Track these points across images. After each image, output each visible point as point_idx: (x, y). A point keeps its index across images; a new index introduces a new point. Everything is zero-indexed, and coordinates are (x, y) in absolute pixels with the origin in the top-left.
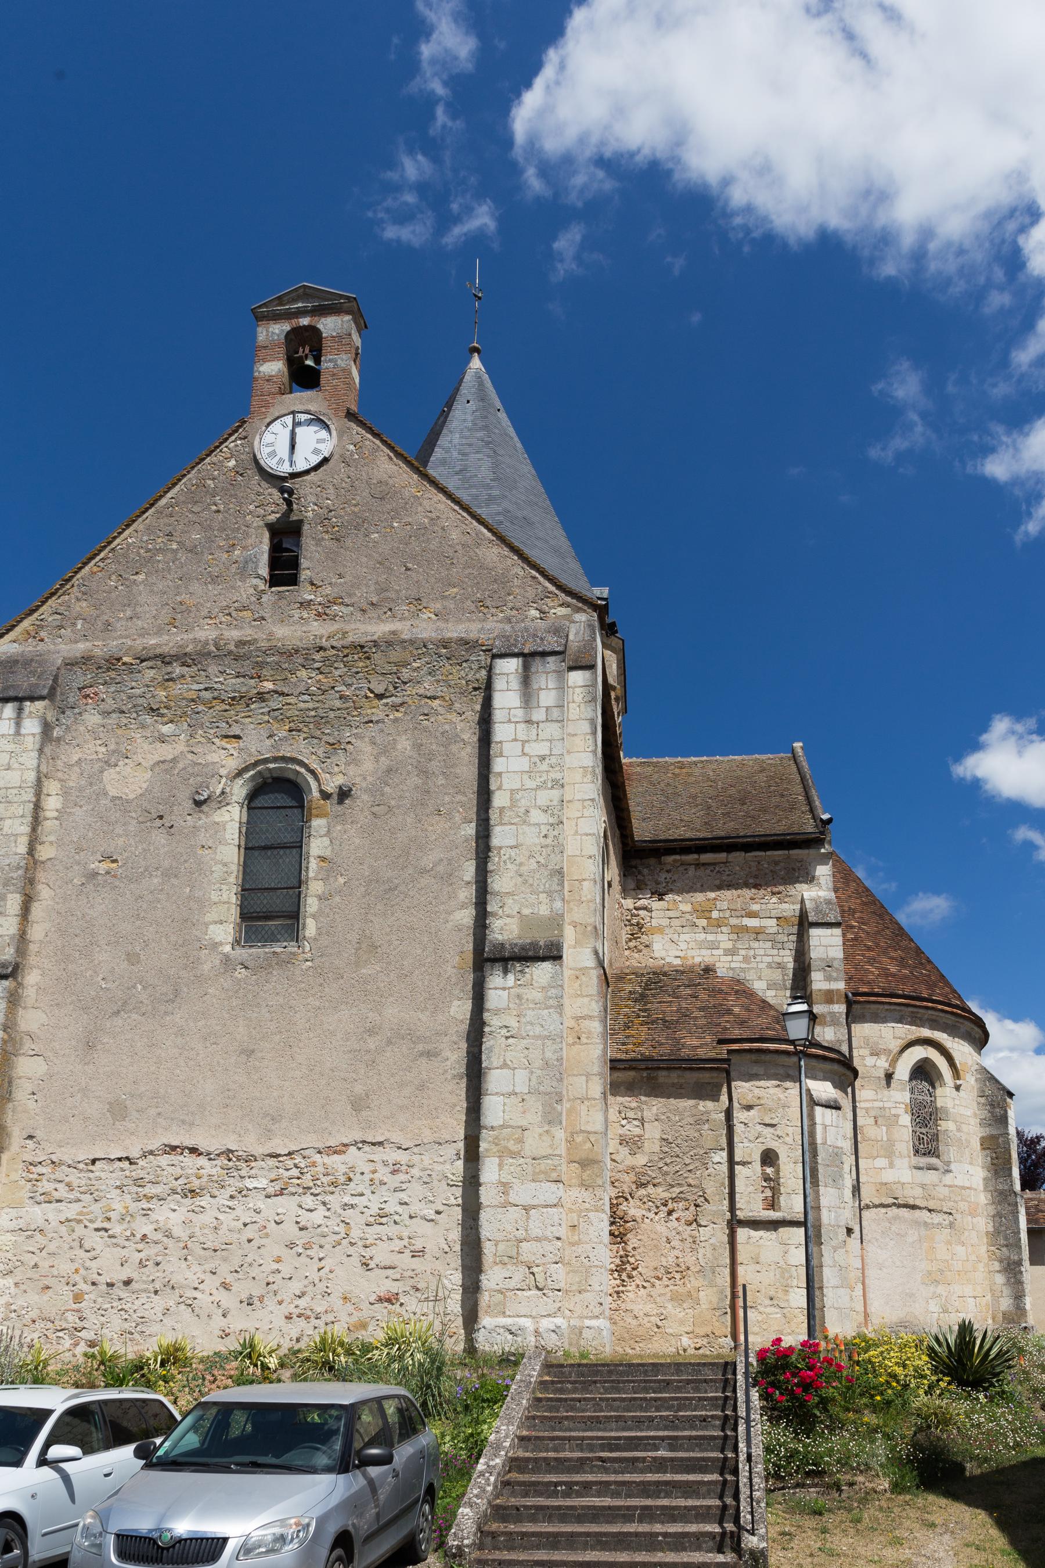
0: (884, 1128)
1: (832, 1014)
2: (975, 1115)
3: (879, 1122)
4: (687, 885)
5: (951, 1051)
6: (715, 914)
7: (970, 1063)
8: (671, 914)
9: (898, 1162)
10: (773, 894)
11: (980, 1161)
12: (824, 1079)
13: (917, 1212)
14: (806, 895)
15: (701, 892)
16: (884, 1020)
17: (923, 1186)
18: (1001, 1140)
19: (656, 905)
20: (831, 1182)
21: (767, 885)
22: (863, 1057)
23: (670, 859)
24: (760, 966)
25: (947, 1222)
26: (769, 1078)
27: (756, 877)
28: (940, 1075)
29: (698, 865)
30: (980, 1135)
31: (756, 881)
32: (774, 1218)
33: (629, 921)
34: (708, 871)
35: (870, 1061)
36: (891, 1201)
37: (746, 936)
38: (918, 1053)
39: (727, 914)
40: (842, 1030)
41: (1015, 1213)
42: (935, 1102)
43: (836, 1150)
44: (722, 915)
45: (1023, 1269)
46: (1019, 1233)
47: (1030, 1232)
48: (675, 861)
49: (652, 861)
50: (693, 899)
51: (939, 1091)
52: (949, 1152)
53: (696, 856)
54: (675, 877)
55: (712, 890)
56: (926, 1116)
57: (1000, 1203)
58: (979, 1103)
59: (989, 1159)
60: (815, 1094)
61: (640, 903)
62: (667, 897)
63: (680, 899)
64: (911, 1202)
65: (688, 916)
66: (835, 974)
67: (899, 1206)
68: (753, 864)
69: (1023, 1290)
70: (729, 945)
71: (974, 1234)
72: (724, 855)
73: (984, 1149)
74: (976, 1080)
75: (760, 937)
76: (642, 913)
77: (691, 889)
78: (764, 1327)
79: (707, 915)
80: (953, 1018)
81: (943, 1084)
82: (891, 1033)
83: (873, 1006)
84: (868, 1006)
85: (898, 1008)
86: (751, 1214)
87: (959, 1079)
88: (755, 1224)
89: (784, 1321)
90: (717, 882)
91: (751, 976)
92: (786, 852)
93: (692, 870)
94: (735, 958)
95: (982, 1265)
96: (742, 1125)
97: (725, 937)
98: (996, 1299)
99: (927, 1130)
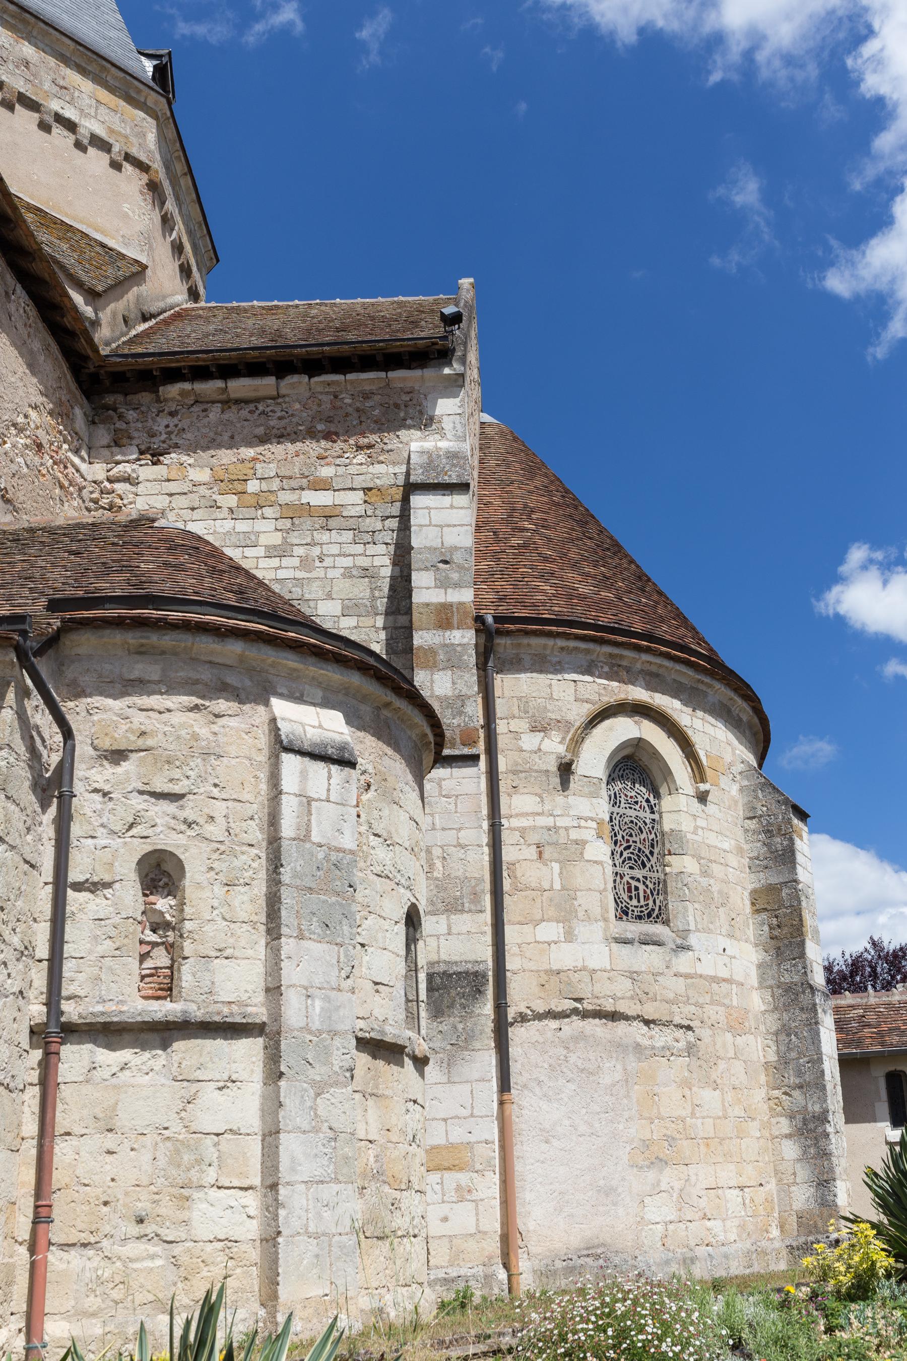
0: (556, 866)
1: (449, 647)
2: (740, 851)
3: (546, 855)
4: (204, 436)
5: (690, 732)
6: (253, 486)
7: (728, 758)
8: (172, 487)
9: (582, 930)
10: (359, 448)
11: (751, 933)
12: (326, 703)
13: (621, 1027)
14: (415, 446)
15: (230, 448)
16: (558, 668)
17: (633, 975)
18: (785, 892)
19: (147, 472)
20: (315, 926)
21: (349, 433)
22: (516, 735)
23: (173, 390)
24: (331, 574)
25: (682, 1044)
26: (172, 689)
27: (329, 420)
28: (667, 773)
29: (227, 403)
30: (750, 887)
31: (329, 427)
32: (159, 1016)
33: (95, 501)
34: (244, 413)
35: (530, 741)
36: (569, 1005)
37: (308, 523)
38: (623, 730)
39: (275, 484)
40: (467, 676)
41: (813, 1024)
42: (660, 822)
43: (334, 856)
44: (265, 487)
45: (830, 1129)
46: (820, 1060)
47: (845, 1062)
48: (183, 393)
49: (145, 398)
50: (214, 460)
51: (667, 803)
52: (687, 913)
53: (220, 384)
54: (185, 423)
55: (250, 445)
56: (641, 852)
57: (786, 1008)
58: (746, 831)
59: (766, 928)
60: (285, 728)
61: (117, 470)
62: (166, 459)
63: (191, 461)
64: (609, 1006)
65: (203, 490)
66: (455, 576)
67: (585, 1015)
68: (324, 398)
69: (831, 1170)
70: (276, 539)
71: (738, 1067)
72: (271, 380)
73: (758, 911)
74: (741, 790)
75: (333, 523)
76: (119, 487)
77: (212, 444)
78: (116, 1294)
79: (239, 487)
80: (690, 672)
81: (674, 790)
82: (570, 693)
83: (535, 641)
84: (525, 641)
85: (582, 645)
86: (99, 1008)
87: (703, 780)
88: (109, 1033)
89: (172, 1274)
90: (260, 431)
91: (313, 591)
92: (382, 374)
93: (215, 412)
94: (286, 562)
95: (756, 1124)
96: (97, 797)
97: (269, 525)
98: (785, 1188)
99: (644, 872)
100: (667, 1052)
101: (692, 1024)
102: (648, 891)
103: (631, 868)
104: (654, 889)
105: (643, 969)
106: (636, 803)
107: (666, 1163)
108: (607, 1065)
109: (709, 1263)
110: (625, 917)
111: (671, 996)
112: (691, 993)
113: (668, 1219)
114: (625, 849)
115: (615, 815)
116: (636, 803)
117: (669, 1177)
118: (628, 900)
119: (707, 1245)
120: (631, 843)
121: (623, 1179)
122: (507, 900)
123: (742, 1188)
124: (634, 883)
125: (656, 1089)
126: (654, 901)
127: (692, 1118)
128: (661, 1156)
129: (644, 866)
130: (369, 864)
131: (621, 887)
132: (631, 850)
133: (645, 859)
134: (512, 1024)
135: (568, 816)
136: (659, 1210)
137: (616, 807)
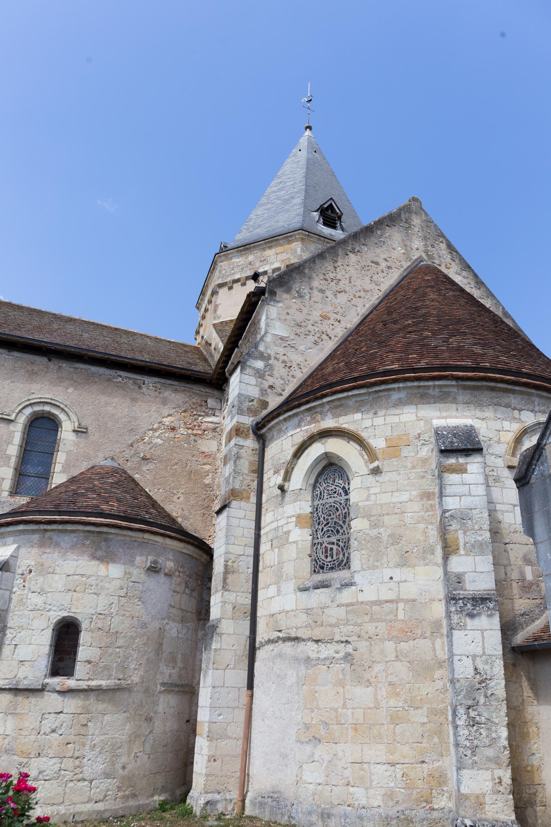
13: (301, 646)
17: (308, 611)
25: (342, 654)
99: (338, 537)
100: (330, 661)
101: (349, 639)
102: (340, 549)
103: (329, 537)
104: (344, 546)
105: (314, 606)
106: (335, 492)
107: (320, 741)
108: (290, 672)
109: (343, 820)
110: (321, 571)
111: (334, 621)
112: (350, 617)
113: (318, 782)
114: (325, 525)
115: (319, 506)
116: (335, 492)
117: (322, 752)
118: (324, 559)
119: (349, 806)
120: (329, 520)
121: (292, 750)
122: (260, 575)
123: (393, 765)
124: (329, 546)
125: (317, 688)
126: (344, 555)
127: (343, 709)
128: (316, 736)
129: (338, 532)
130: (26, 607)
131: (321, 551)
132: (329, 525)
133: (339, 528)
134: (259, 648)
135: (283, 518)
136: (312, 775)
137: (321, 501)
